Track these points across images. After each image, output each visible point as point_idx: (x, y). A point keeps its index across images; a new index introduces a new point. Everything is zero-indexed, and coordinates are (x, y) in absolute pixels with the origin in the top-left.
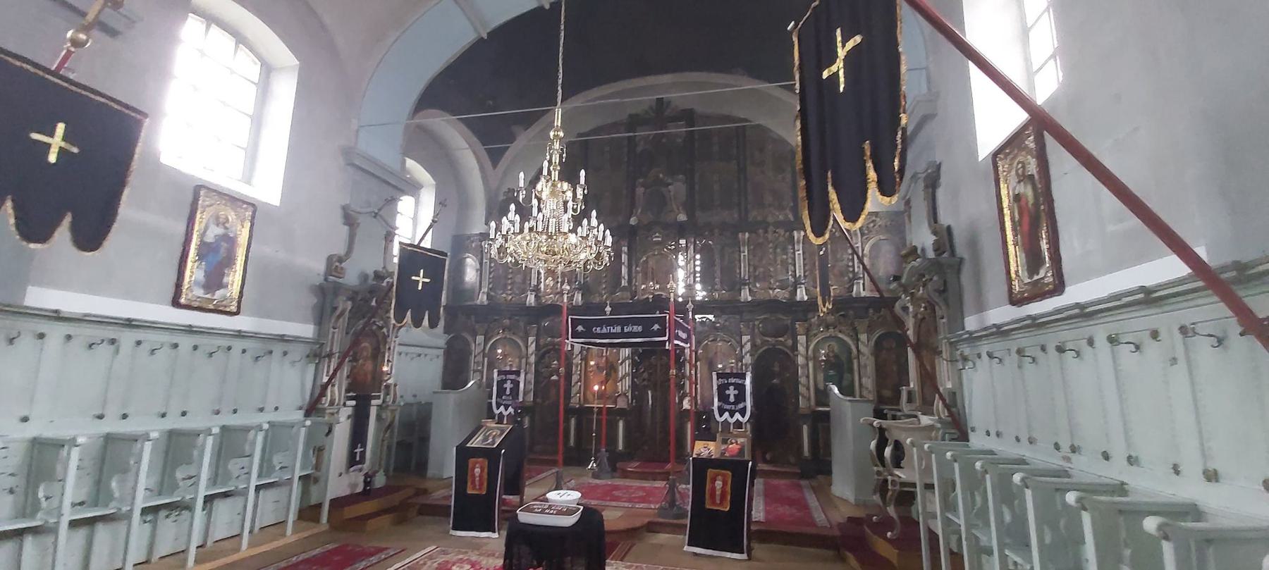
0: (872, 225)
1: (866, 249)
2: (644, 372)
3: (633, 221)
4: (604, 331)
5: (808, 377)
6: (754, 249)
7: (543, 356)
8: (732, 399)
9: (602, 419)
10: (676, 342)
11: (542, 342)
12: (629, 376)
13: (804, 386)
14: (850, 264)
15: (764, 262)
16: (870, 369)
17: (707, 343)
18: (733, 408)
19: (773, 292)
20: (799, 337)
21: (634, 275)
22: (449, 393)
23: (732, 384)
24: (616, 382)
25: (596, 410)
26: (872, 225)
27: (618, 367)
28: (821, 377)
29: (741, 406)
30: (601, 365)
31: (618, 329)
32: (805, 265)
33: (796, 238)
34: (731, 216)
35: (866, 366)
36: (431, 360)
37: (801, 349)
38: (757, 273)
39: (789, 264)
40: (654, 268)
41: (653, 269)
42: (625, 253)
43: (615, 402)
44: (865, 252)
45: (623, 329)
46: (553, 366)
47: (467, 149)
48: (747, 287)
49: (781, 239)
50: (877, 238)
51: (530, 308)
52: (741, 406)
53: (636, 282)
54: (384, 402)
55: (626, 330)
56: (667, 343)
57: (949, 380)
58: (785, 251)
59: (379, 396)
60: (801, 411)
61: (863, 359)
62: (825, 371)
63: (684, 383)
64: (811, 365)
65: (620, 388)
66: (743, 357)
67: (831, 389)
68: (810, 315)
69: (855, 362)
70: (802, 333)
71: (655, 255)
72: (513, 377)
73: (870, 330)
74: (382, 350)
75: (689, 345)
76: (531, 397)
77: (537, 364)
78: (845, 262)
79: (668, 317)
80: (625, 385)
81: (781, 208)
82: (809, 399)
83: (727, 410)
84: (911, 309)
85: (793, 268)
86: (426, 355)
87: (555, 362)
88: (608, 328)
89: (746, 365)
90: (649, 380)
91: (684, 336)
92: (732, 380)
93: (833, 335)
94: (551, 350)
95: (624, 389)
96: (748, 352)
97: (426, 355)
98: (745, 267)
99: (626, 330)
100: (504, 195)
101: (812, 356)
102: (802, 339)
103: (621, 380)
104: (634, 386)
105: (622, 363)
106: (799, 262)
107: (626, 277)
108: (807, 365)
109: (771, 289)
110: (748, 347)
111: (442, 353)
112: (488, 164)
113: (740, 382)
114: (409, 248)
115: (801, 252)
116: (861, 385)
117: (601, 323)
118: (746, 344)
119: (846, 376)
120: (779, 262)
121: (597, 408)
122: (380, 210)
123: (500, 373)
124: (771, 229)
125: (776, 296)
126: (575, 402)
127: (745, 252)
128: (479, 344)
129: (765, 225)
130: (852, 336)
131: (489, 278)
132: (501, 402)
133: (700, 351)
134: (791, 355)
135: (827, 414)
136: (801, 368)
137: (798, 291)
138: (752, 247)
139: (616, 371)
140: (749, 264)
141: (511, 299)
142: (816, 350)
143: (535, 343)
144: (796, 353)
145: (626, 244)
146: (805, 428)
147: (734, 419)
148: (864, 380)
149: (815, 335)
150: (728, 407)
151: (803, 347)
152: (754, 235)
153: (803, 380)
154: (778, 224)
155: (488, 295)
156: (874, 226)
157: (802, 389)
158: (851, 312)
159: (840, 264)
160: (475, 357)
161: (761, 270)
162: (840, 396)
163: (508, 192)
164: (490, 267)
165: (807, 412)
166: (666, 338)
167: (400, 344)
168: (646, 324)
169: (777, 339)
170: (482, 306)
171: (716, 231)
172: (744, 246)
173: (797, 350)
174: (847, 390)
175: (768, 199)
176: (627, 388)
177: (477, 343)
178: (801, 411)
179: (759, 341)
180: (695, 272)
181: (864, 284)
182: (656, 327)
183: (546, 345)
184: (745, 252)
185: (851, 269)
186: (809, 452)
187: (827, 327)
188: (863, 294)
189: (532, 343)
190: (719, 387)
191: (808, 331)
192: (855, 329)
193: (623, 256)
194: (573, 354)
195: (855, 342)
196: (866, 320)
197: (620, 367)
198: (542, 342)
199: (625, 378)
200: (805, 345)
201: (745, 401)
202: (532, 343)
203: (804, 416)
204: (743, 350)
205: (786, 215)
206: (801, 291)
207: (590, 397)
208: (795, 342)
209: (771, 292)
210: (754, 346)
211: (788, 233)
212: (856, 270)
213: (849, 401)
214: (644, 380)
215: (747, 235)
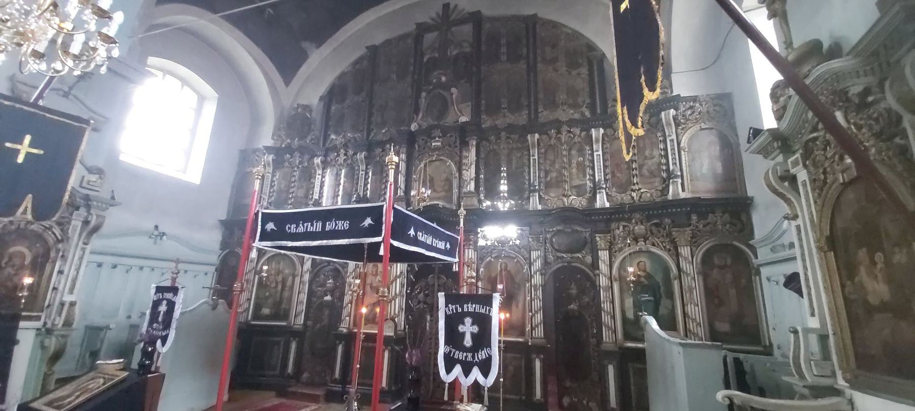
0: (689, 112)
1: (683, 141)
2: (419, 293)
3: (414, 127)
4: (301, 229)
5: (613, 302)
6: (546, 151)
8: (468, 342)
14: (663, 161)
15: (557, 166)
16: (698, 293)
17: (490, 261)
18: (470, 358)
23: (469, 314)
26: (689, 112)
28: (629, 302)
29: (482, 355)
31: (318, 227)
32: (605, 167)
34: (522, 118)
35: (691, 290)
37: (603, 267)
38: (549, 179)
39: (585, 167)
44: (682, 145)
45: (324, 226)
46: (328, 285)
48: (537, 194)
49: (576, 139)
50: (697, 127)
52: (482, 355)
55: (328, 228)
57: (813, 315)
58: (581, 152)
60: (604, 347)
61: (686, 281)
62: (634, 294)
66: (532, 276)
67: (646, 322)
68: (613, 225)
69: (676, 284)
72: (169, 296)
73: (694, 243)
77: (311, 282)
78: (656, 160)
80: (397, 307)
81: (575, 106)
82: (615, 331)
83: (458, 361)
84: (802, 176)
85: (591, 172)
86: (186, 271)
87: (330, 281)
89: (535, 286)
90: (425, 303)
93: (644, 249)
95: (392, 313)
96: (537, 271)
97: (186, 271)
98: (535, 172)
101: (617, 276)
102: (604, 255)
103: (391, 302)
104: (408, 310)
106: (599, 164)
109: (564, 195)
110: (538, 265)
113: (483, 311)
114: (6, 103)
115: (600, 153)
116: (685, 315)
118: (535, 261)
119: (665, 302)
120: (574, 165)
122: (71, 88)
124: (565, 128)
126: (343, 328)
127: (535, 154)
129: (557, 124)
130: (670, 250)
133: (482, 269)
134: (591, 274)
135: (642, 351)
137: (598, 196)
138: (543, 151)
142: (622, 267)
144: (597, 272)
145: (404, 152)
146: (611, 370)
147: (471, 380)
148: (690, 309)
149: (621, 250)
150: (460, 355)
152: (544, 137)
153: (606, 306)
154: (572, 123)
156: (693, 113)
157: (606, 319)
158: (667, 221)
159: (649, 162)
161: (554, 175)
162: (662, 333)
167: (92, 253)
169: (574, 255)
171: (503, 134)
172: (533, 147)
173: (598, 269)
174: (668, 324)
175: (562, 97)
178: (604, 347)
179: (551, 257)
181: (683, 184)
182: (368, 221)
184: (535, 154)
185: (664, 168)
187: (636, 240)
188: (683, 195)
190: (448, 318)
191: (610, 247)
192: (673, 242)
194: (347, 272)
195: (675, 258)
196: (688, 229)
203: (609, 354)
205: (583, 114)
206: (602, 198)
208: (596, 259)
209: (565, 200)
210: (546, 263)
211: (584, 133)
212: (671, 167)
213: (681, 344)
214: (419, 302)
215: (537, 136)
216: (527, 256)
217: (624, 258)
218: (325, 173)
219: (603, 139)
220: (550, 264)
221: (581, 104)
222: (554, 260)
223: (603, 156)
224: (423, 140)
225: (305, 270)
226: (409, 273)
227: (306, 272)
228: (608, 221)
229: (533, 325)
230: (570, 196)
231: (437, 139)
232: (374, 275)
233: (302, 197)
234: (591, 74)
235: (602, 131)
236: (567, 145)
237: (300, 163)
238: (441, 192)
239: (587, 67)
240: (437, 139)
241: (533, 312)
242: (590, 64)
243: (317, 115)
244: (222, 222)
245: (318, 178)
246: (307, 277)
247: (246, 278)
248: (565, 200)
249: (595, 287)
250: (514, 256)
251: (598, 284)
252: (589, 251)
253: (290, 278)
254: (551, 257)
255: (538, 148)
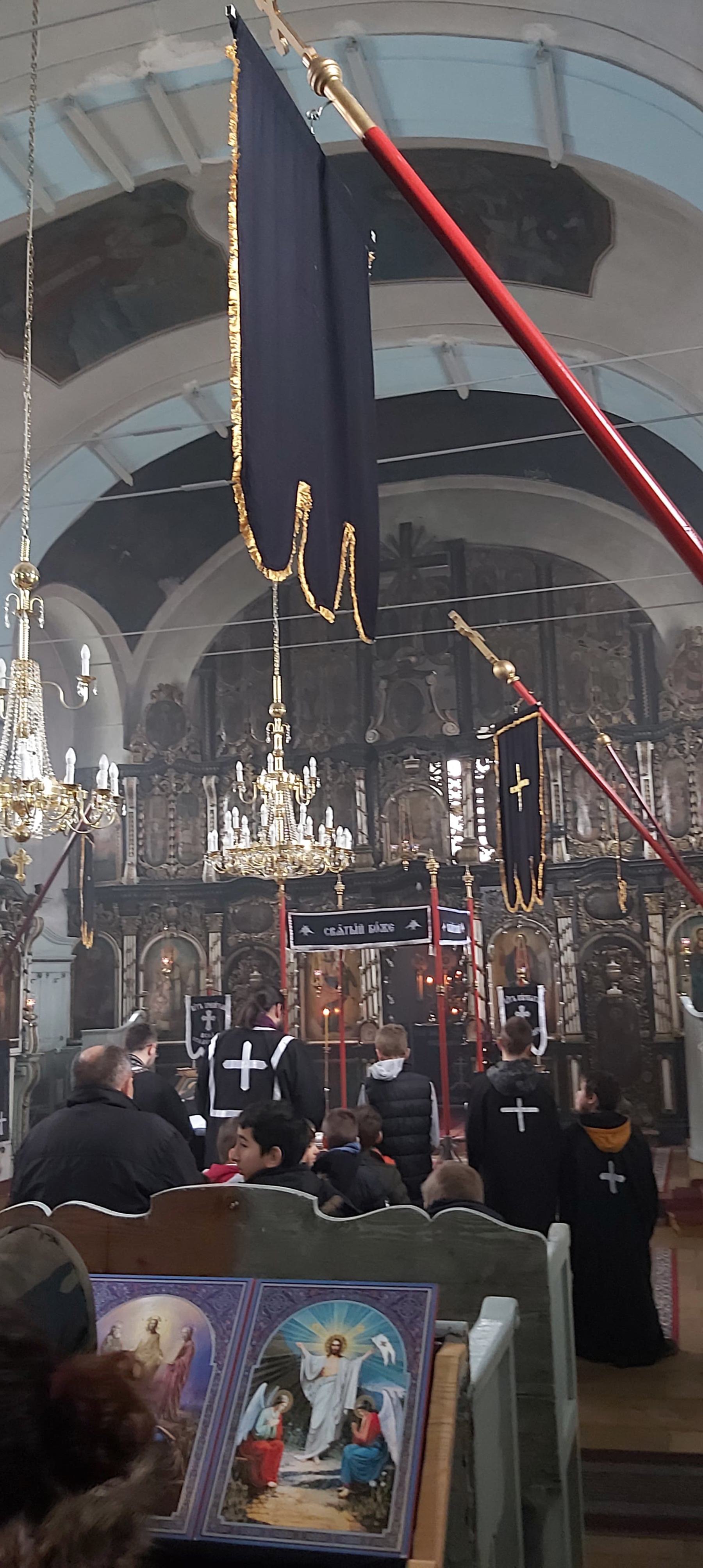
3: (371, 737)
4: (341, 932)
5: (667, 982)
6: (573, 773)
7: (234, 965)
9: (338, 1065)
10: (443, 943)
11: (231, 940)
12: (378, 989)
13: (662, 997)
17: (502, 933)
19: (606, 844)
20: (650, 918)
21: (377, 825)
22: (106, 1033)
23: (522, 1003)
24: (357, 1001)
25: (327, 1049)
27: (359, 978)
30: (331, 975)
31: (360, 930)
33: (639, 754)
36: (55, 981)
37: (655, 938)
40: (409, 813)
41: (406, 815)
42: (360, 790)
43: (358, 1036)
45: (366, 929)
47: (96, 637)
48: (562, 839)
51: (210, 885)
53: (381, 836)
54: (24, 1051)
55: (371, 931)
56: (431, 947)
59: (17, 1042)
60: (657, 1039)
63: (467, 1000)
64: (671, 962)
65: (365, 1009)
70: (655, 910)
71: (409, 792)
72: (214, 1005)
74: (17, 975)
75: (469, 940)
76: (575, 1026)
79: (429, 910)
82: (670, 1019)
87: (256, 973)
88: (346, 928)
89: (566, 966)
91: (458, 929)
92: (522, 998)
94: (247, 953)
97: (47, 975)
99: (371, 931)
100: (153, 697)
101: (672, 949)
102: (656, 921)
105: (365, 972)
107: (365, 831)
108: (666, 963)
109: (601, 839)
110: (569, 936)
111: (69, 970)
112: (123, 648)
113: (532, 1000)
117: (336, 921)
118: (564, 931)
121: (330, 1045)
123: (194, 1001)
125: (611, 851)
128: (129, 950)
131: (138, 839)
132: (200, 1042)
133: (491, 946)
136: (657, 968)
139: (357, 985)
140: (564, 801)
141: (176, 873)
142: (677, 939)
143: (219, 943)
144: (647, 943)
145: (362, 776)
151: (659, 934)
155: (138, 866)
160: (123, 971)
163: (160, 690)
164: (139, 821)
165: (667, 1039)
166: (428, 940)
168: (400, 919)
170: (130, 887)
173: (649, 940)
176: (376, 1012)
177: (125, 949)
179: (585, 926)
180: (476, 817)
182: (414, 924)
183: (240, 945)
186: (673, 1104)
189: (215, 943)
193: (358, 793)
197: (363, 977)
198: (231, 940)
199: (372, 995)
200: (661, 932)
201: (538, 1026)
202: (215, 943)
204: (560, 940)
205: (624, 717)
207: (315, 1027)
209: (602, 844)
210: (578, 934)
211: (626, 747)
216: (553, 925)
217: (679, 928)
218: (222, 802)
219: (653, 757)
220: (584, 934)
221: (621, 701)
222: (591, 930)
223: (654, 781)
224: (389, 758)
225: (214, 960)
226: (384, 956)
227: (215, 963)
228: (660, 876)
229: (567, 1018)
230: (610, 839)
231: (412, 758)
232: (329, 961)
233: (189, 844)
234: (635, 656)
235: (651, 746)
236: (603, 765)
237: (179, 787)
238: (425, 837)
239: (630, 644)
240: (412, 758)
241: (565, 1000)
242: (633, 636)
243: (188, 700)
244: (64, 890)
245: (212, 811)
246: (217, 970)
247: (125, 978)
248: (602, 844)
249: (646, 964)
250: (535, 926)
251: (648, 960)
252: (636, 915)
253: (192, 974)
254: (585, 926)
255: (562, 768)
